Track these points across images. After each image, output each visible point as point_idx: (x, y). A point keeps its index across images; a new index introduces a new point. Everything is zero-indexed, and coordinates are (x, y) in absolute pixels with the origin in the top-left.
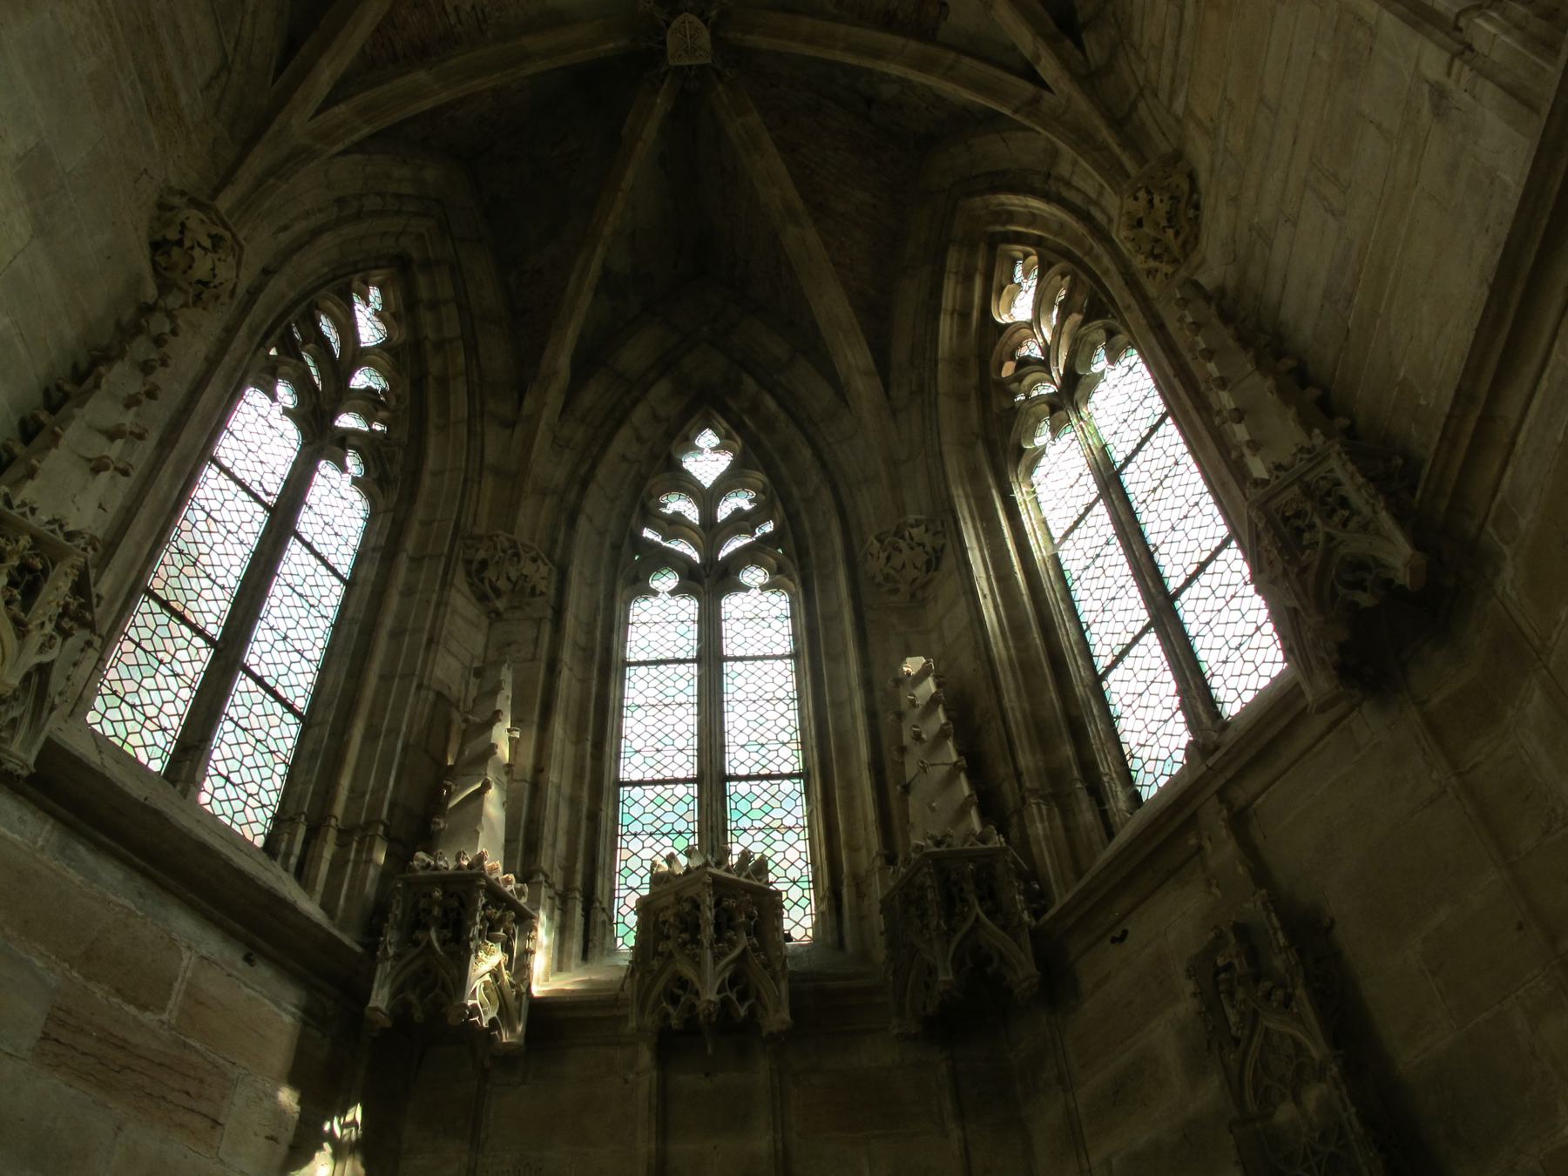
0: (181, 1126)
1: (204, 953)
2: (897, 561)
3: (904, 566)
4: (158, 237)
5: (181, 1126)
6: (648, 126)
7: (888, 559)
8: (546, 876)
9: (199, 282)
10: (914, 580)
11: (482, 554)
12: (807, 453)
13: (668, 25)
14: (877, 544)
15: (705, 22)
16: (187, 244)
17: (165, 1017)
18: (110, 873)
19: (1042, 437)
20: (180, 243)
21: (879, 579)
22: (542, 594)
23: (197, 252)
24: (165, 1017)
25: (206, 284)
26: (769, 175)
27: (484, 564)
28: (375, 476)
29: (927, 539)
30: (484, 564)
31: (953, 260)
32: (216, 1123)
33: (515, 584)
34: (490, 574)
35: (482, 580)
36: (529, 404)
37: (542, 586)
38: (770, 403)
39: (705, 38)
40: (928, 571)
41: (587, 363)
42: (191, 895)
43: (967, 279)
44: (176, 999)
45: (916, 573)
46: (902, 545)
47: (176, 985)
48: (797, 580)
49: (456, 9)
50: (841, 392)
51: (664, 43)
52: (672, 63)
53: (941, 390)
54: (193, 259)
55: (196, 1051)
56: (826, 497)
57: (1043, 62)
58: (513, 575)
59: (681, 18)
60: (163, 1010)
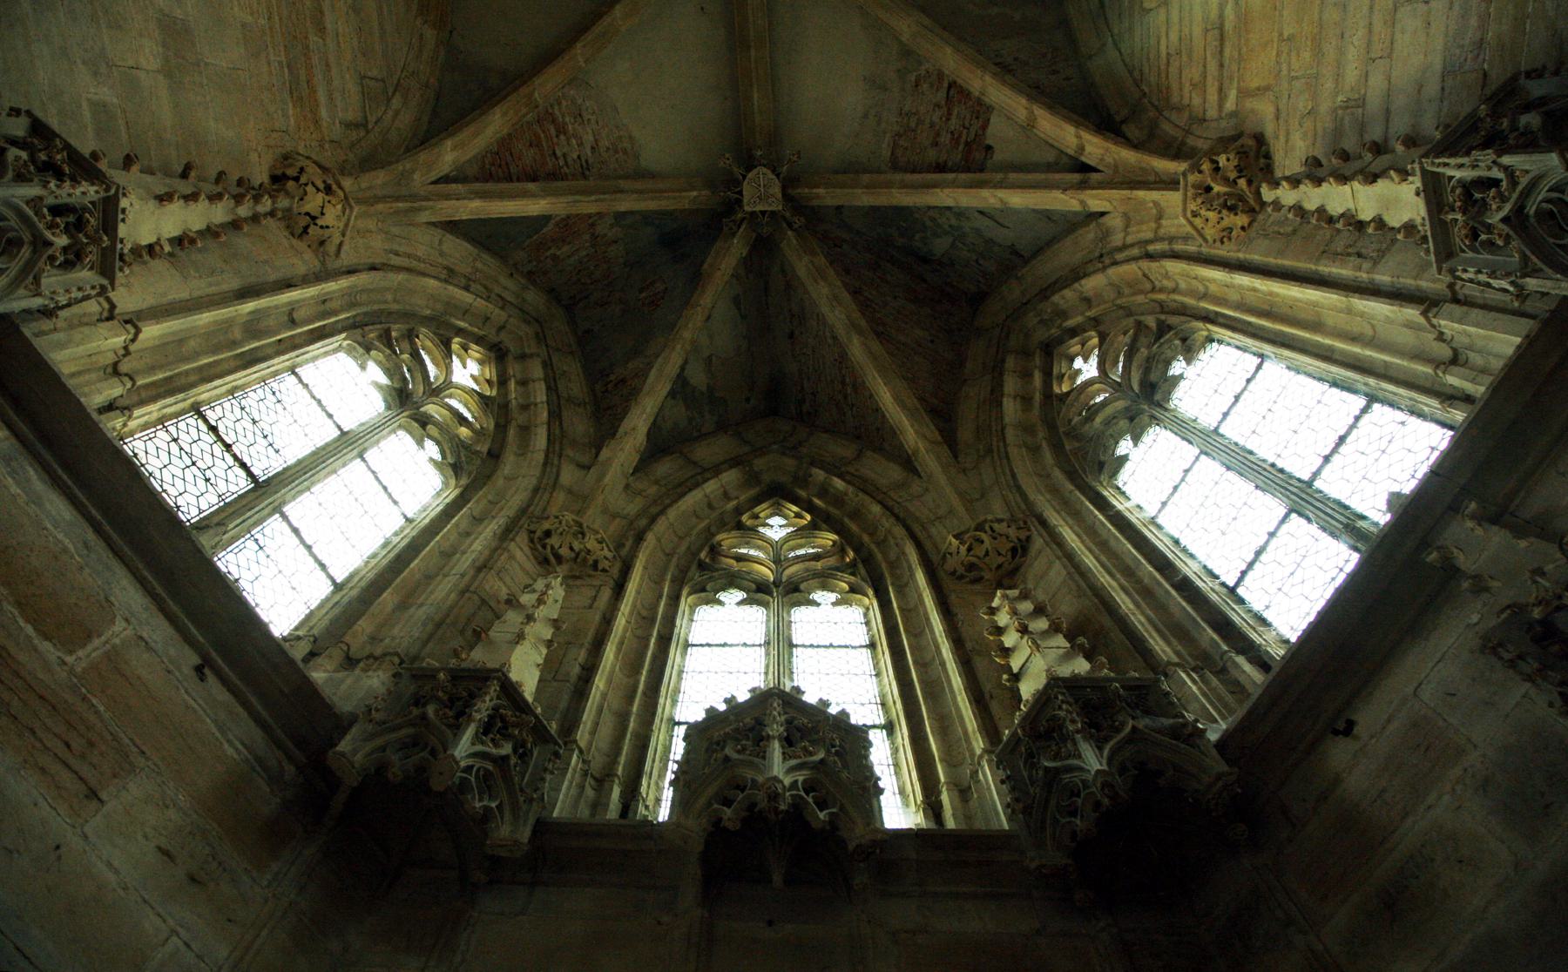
0: (43, 770)
1: (145, 635)
2: (980, 551)
3: (987, 554)
4: (279, 172)
5: (43, 770)
6: (729, 256)
7: (969, 550)
8: (581, 751)
9: (307, 214)
10: (999, 566)
11: (546, 526)
12: (876, 509)
13: (744, 177)
14: (955, 542)
15: (778, 176)
16: (303, 180)
17: (70, 659)
18: (57, 507)
19: (1124, 446)
20: (297, 179)
21: (961, 570)
22: (604, 570)
23: (310, 189)
24: (70, 659)
25: (314, 218)
26: (829, 302)
27: (548, 534)
28: (450, 460)
29: (1012, 532)
30: (548, 534)
31: (1010, 362)
32: (93, 794)
33: (578, 554)
34: (554, 541)
35: (544, 547)
36: (605, 453)
37: (604, 564)
38: (839, 484)
39: (776, 190)
40: (1013, 557)
41: (659, 446)
42: (146, 573)
43: (1026, 375)
44: (93, 650)
45: (1000, 560)
46: (983, 536)
47: (96, 642)
48: (870, 592)
49: (564, 155)
50: (908, 463)
51: (740, 193)
52: (747, 208)
53: (1007, 420)
54: (306, 193)
55: (97, 712)
56: (899, 531)
57: (1088, 149)
58: (576, 546)
59: (755, 171)
60: (71, 653)
